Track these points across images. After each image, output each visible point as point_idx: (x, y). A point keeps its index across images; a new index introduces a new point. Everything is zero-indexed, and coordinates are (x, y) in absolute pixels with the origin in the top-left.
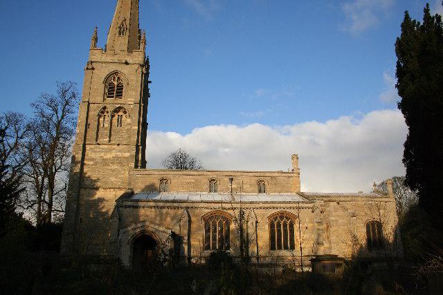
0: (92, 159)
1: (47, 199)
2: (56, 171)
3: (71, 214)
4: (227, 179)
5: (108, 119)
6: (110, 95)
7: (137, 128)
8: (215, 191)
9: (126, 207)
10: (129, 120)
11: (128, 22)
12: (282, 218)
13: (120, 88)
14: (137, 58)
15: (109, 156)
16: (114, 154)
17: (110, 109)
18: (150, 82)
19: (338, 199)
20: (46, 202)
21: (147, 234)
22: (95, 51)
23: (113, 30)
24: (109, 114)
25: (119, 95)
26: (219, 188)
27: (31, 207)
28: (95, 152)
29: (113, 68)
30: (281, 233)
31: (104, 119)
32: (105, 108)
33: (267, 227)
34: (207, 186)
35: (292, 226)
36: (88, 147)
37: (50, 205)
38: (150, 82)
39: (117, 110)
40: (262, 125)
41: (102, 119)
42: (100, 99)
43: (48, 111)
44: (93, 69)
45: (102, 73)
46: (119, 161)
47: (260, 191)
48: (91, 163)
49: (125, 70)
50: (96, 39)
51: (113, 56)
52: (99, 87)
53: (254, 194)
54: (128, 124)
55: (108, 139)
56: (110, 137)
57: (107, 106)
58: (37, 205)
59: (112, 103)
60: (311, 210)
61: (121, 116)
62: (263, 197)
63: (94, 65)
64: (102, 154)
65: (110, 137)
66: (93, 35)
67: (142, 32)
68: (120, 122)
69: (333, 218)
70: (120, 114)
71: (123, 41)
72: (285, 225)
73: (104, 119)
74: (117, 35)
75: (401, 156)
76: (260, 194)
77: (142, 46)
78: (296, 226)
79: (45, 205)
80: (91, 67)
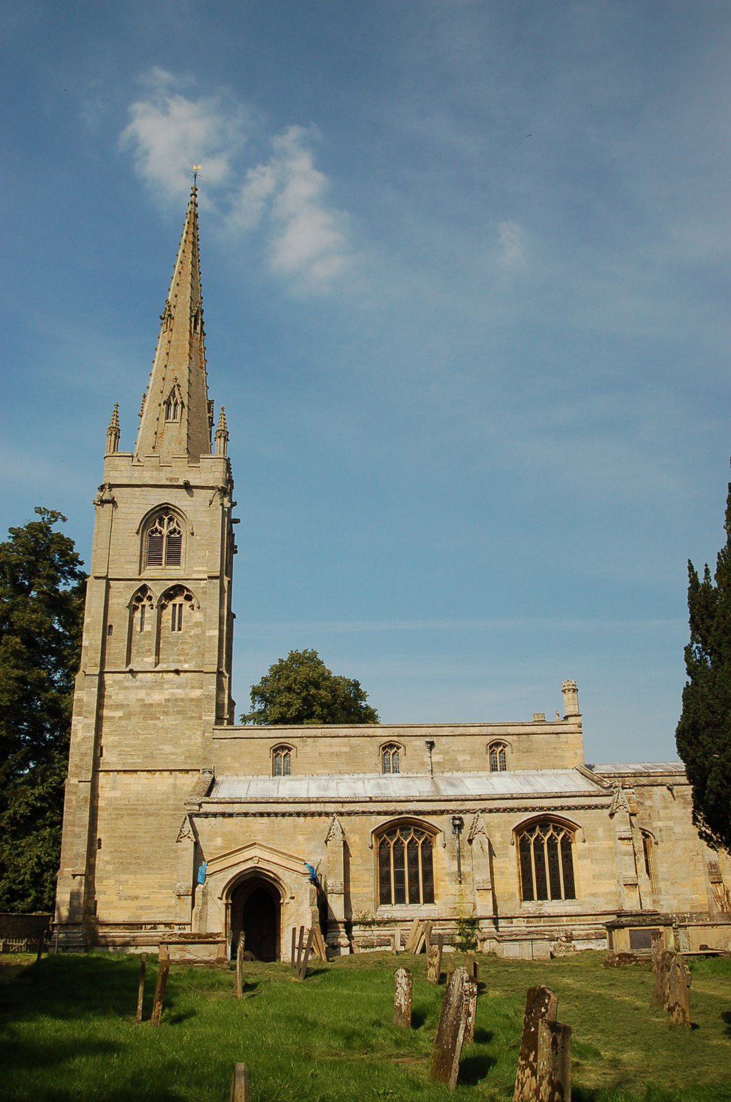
0: (118, 707)
3: (76, 829)
4: (421, 743)
5: (151, 614)
6: (154, 559)
7: (216, 633)
8: (396, 771)
9: (206, 815)
10: (198, 616)
11: (185, 387)
12: (544, 827)
14: (209, 473)
15: (157, 697)
16: (167, 694)
17: (156, 591)
18: (237, 521)
19: (669, 780)
22: (117, 461)
23: (152, 408)
24: (155, 602)
25: (174, 557)
26: (403, 764)
28: (126, 688)
31: (143, 613)
32: (144, 589)
33: (513, 852)
34: (376, 760)
35: (428, 846)
36: (108, 678)
39: (169, 595)
41: (138, 615)
42: (131, 570)
44: (113, 502)
45: (135, 507)
46: (176, 706)
47: (494, 769)
48: (119, 714)
50: (116, 433)
52: (132, 545)
53: (481, 773)
54: (197, 624)
55: (152, 659)
56: (157, 653)
57: (149, 584)
59: (161, 576)
60: (607, 812)
61: (181, 605)
62: (502, 784)
64: (142, 694)
65: (157, 653)
66: (108, 422)
67: (216, 408)
68: (177, 624)
69: (660, 824)
70: (179, 600)
71: (177, 431)
72: (538, 847)
73: (143, 613)
74: (162, 420)
75: (673, 712)
76: (495, 773)
77: (218, 444)
78: (577, 847)
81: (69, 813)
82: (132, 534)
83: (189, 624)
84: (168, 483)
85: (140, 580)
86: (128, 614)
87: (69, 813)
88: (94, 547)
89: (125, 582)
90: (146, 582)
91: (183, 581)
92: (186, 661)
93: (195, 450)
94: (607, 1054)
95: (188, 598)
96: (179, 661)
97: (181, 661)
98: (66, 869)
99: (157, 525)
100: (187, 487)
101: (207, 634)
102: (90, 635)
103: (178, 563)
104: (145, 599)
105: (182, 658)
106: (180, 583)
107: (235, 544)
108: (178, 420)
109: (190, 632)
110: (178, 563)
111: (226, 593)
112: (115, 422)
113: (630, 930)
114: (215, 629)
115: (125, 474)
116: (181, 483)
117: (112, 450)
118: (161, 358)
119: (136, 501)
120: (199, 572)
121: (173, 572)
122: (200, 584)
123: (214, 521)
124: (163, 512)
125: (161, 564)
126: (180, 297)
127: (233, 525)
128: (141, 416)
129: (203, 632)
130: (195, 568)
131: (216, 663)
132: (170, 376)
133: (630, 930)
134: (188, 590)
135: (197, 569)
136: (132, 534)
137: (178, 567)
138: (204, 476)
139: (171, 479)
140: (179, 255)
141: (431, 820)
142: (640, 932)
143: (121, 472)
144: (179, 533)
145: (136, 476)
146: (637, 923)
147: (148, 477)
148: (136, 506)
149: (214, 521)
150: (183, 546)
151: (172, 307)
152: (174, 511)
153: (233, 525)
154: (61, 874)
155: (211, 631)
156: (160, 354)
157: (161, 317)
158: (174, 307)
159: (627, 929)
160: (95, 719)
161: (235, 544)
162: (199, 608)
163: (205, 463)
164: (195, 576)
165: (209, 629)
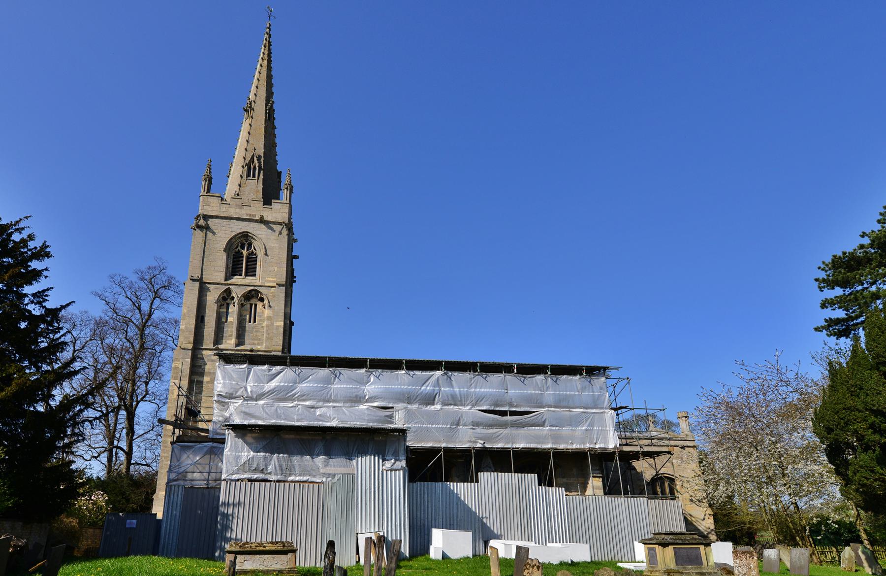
1: (124, 445)
2: (138, 402)
10: (267, 312)
13: (252, 260)
18: (296, 257)
20: (122, 449)
21: (347, 457)
22: (210, 199)
23: (237, 169)
25: (251, 271)
27: (96, 457)
29: (239, 227)
30: (418, 493)
37: (129, 454)
38: (296, 257)
40: (154, 502)
42: (220, 277)
43: (124, 305)
44: (207, 228)
45: (224, 233)
49: (258, 231)
51: (241, 208)
57: (232, 288)
58: (106, 454)
59: (241, 284)
61: (256, 305)
63: (211, 222)
71: (255, 186)
74: (245, 178)
79: (121, 453)
80: (203, 224)
81: (165, 451)
82: (220, 252)
83: (262, 318)
84: (248, 217)
85: (225, 285)
86: (216, 308)
87: (165, 451)
88: (191, 260)
89: (215, 285)
90: (230, 286)
91: (258, 287)
92: (258, 344)
93: (270, 195)
94: (13, 231)
95: (262, 300)
96: (254, 344)
97: (256, 344)
98: (160, 493)
99: (239, 248)
100: (262, 221)
101: (275, 324)
102: (186, 321)
103: (254, 275)
104: (229, 300)
105: (256, 342)
106: (255, 288)
107: (295, 275)
108: (256, 178)
109: (262, 324)
110: (254, 275)
111: (288, 296)
112: (208, 172)
113: (674, 548)
114: (281, 321)
115: (215, 209)
116: (258, 218)
117: (206, 191)
118: (244, 136)
119: (223, 228)
120: (270, 281)
121: (252, 281)
122: (270, 290)
123: (282, 246)
124: (245, 239)
125: (241, 275)
126: (256, 92)
127: (294, 260)
128: (228, 177)
129: (272, 324)
130: (267, 279)
131: (282, 345)
132: (250, 148)
133: (674, 548)
134: (261, 293)
135: (269, 279)
136: (220, 252)
137: (254, 278)
138: (274, 215)
139: (250, 215)
140: (258, 68)
141: (62, 339)
142: (684, 550)
143: (210, 206)
144: (255, 254)
145: (223, 210)
146: (680, 542)
147: (232, 212)
148: (223, 232)
149: (282, 246)
150: (258, 263)
151: (253, 103)
152: (252, 238)
153: (294, 260)
154: (157, 497)
155: (278, 323)
156: (243, 134)
157: (244, 109)
158: (254, 101)
159: (671, 548)
160: (187, 381)
161: (295, 275)
162: (270, 306)
163: (275, 205)
164: (267, 284)
165: (276, 321)
